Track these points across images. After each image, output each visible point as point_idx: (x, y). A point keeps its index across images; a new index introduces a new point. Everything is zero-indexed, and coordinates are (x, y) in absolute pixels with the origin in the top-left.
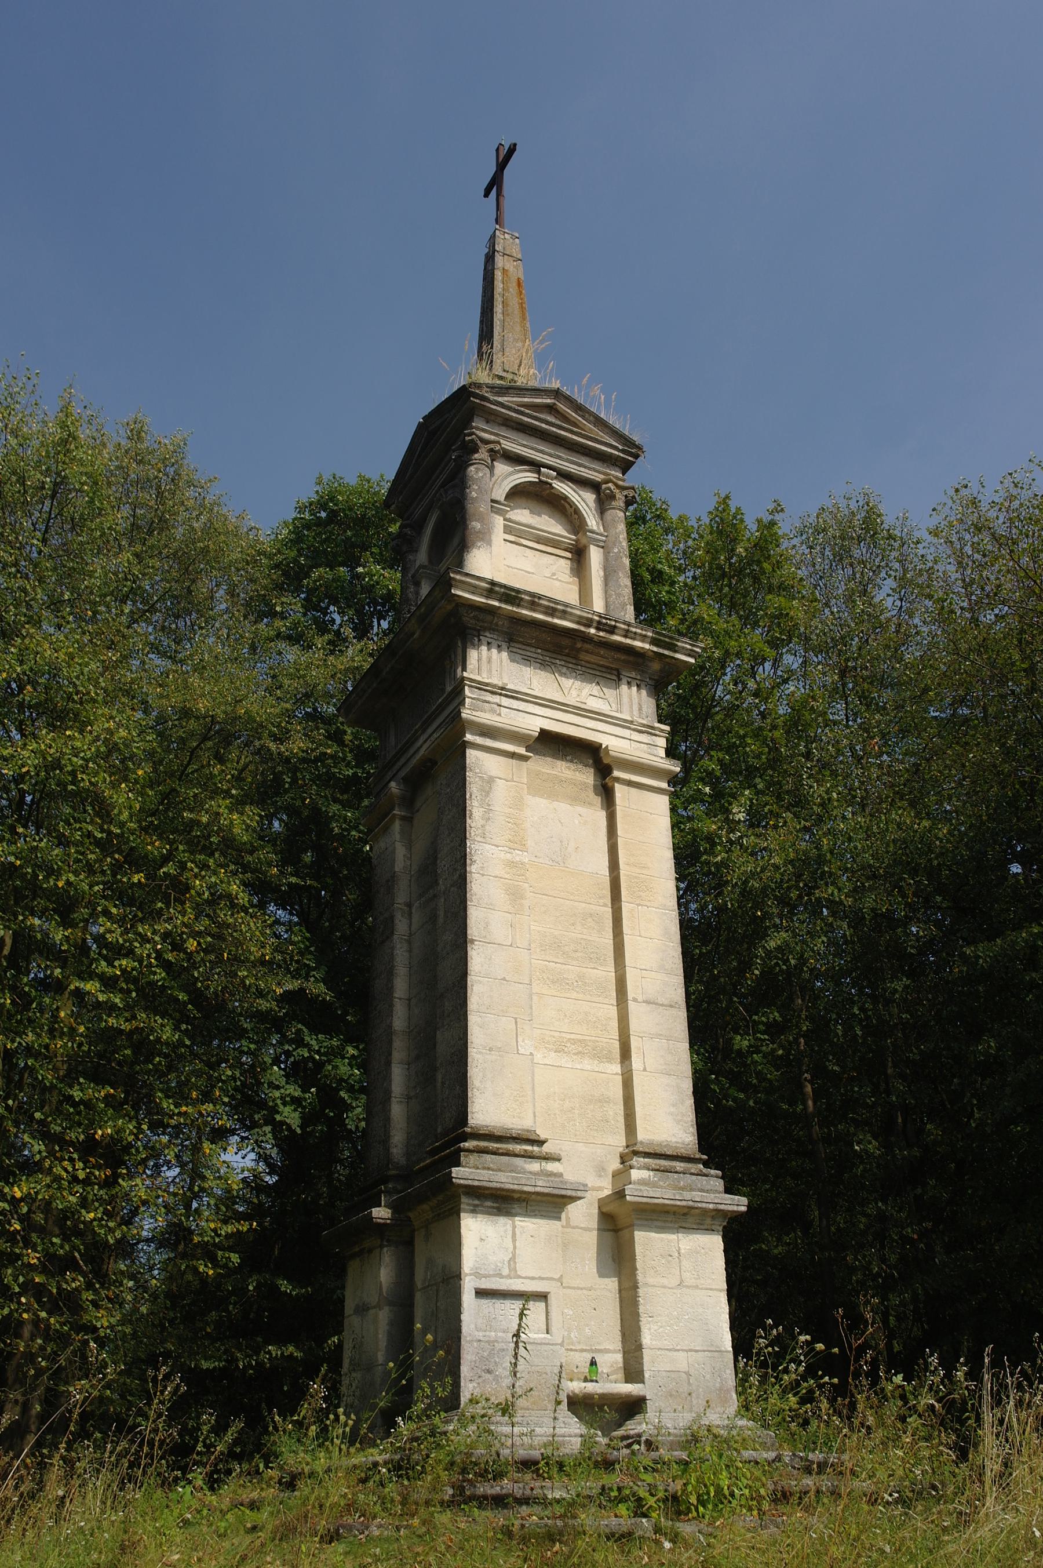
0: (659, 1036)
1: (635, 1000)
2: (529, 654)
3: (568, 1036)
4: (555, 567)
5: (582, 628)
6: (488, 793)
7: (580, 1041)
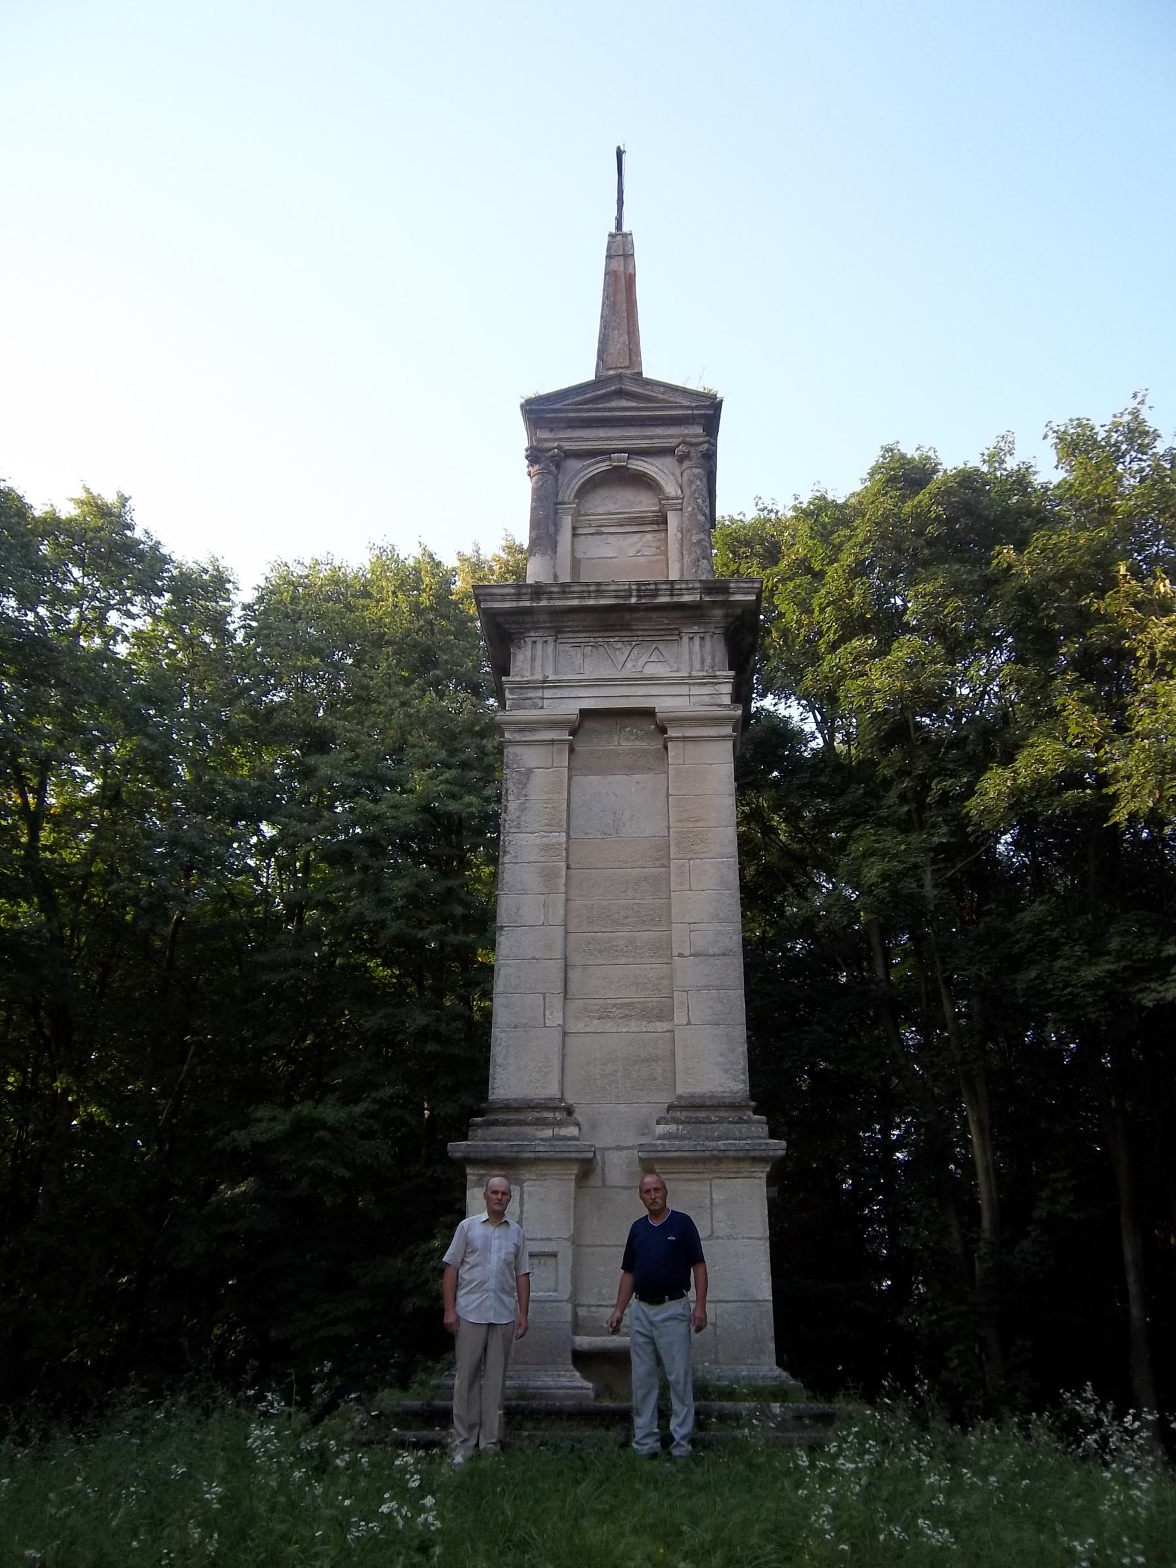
0: (707, 987)
1: (681, 955)
2: (579, 640)
3: (613, 1001)
4: (640, 545)
5: (622, 601)
6: (525, 785)
7: (627, 1004)
